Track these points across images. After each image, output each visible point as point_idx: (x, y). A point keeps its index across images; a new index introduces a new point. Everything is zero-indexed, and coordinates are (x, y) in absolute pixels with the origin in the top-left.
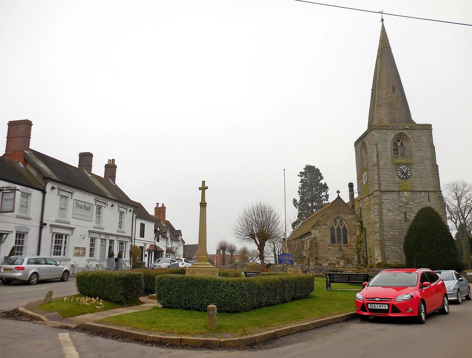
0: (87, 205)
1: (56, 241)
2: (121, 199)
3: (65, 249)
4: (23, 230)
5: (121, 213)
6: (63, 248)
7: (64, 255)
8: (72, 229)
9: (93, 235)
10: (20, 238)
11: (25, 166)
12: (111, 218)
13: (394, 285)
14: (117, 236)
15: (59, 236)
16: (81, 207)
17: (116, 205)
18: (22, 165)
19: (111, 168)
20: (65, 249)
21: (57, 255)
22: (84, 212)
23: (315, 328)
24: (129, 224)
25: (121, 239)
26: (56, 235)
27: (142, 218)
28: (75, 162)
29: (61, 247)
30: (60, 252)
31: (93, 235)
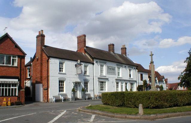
0: (113, 68)
1: (101, 84)
2: (130, 65)
3: (105, 88)
4: (62, 80)
5: (130, 70)
6: (104, 87)
7: (105, 90)
8: (107, 79)
9: (118, 81)
10: (61, 83)
11: (85, 54)
12: (123, 72)
13: (98, 87)
14: (129, 81)
15: (102, 82)
16: (110, 69)
17: (127, 66)
18: (84, 54)
19: (124, 49)
20: (105, 88)
21: (61, 91)
22: (112, 71)
23: (181, 95)
24: (134, 74)
25: (132, 82)
26: (101, 82)
27: (141, 72)
28: (106, 49)
29: (103, 87)
30: (103, 89)
31: (118, 81)
